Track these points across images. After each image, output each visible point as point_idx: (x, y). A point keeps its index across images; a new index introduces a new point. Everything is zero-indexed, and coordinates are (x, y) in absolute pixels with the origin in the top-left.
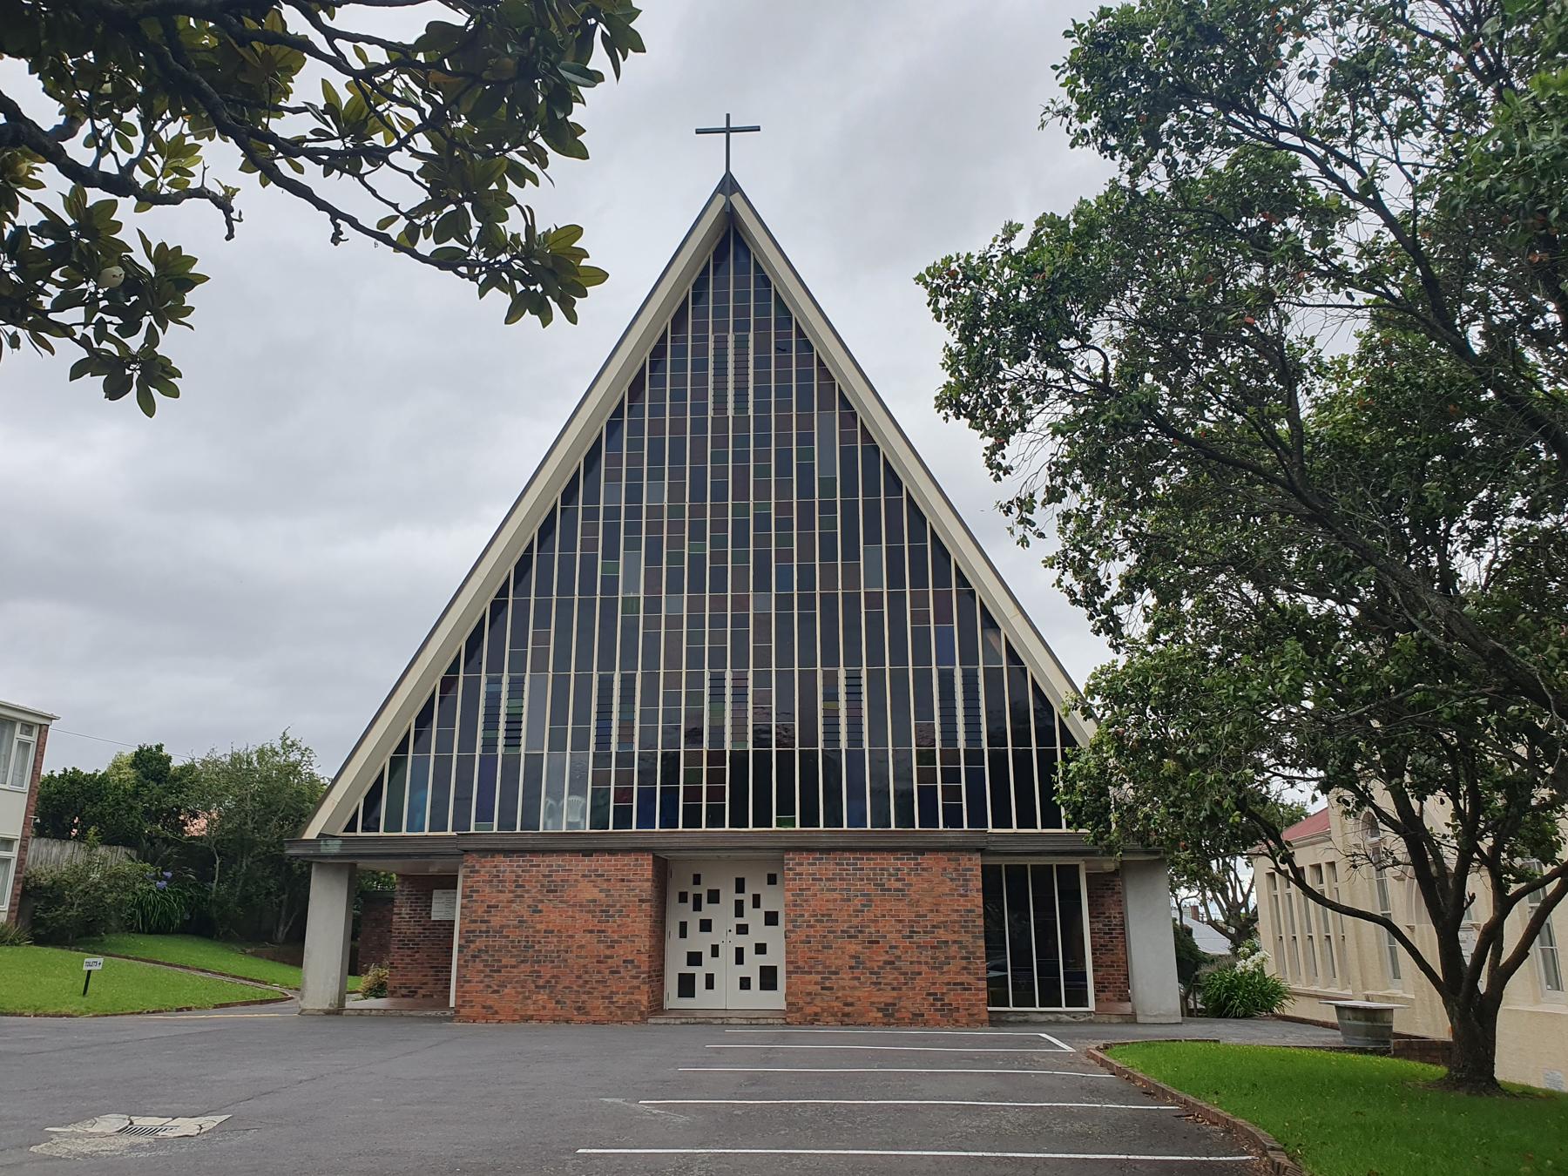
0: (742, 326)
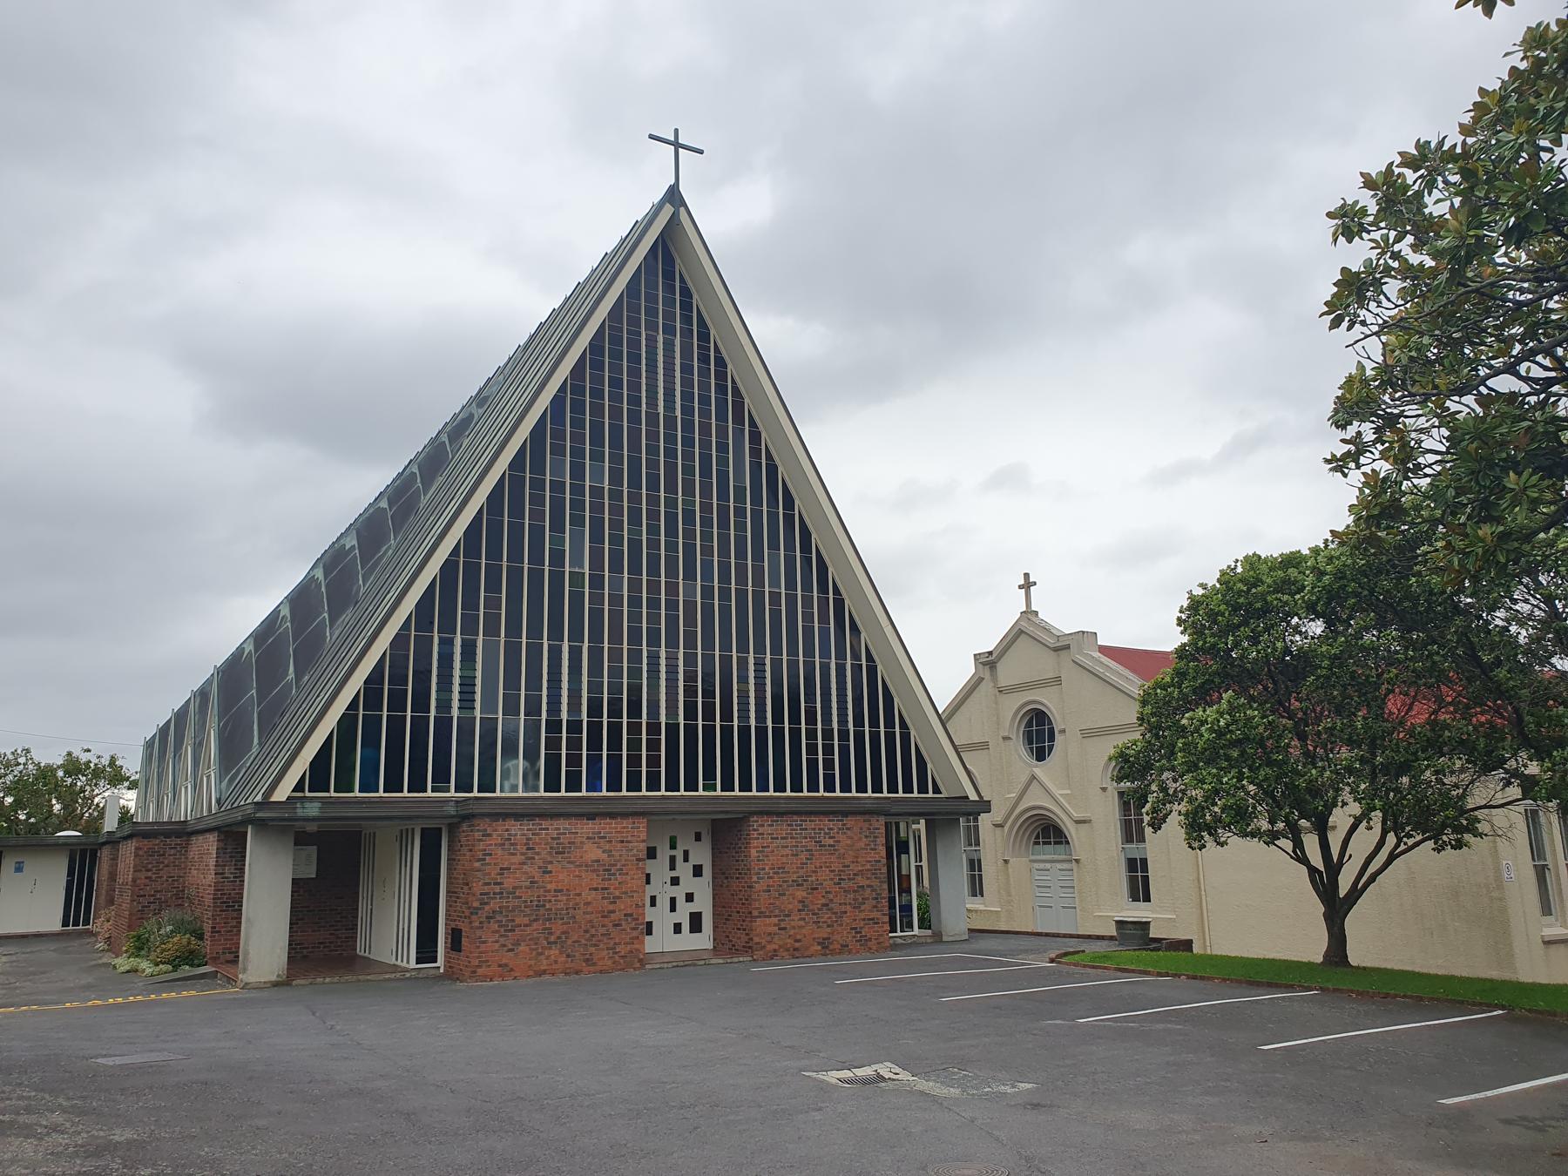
0: (669, 330)
